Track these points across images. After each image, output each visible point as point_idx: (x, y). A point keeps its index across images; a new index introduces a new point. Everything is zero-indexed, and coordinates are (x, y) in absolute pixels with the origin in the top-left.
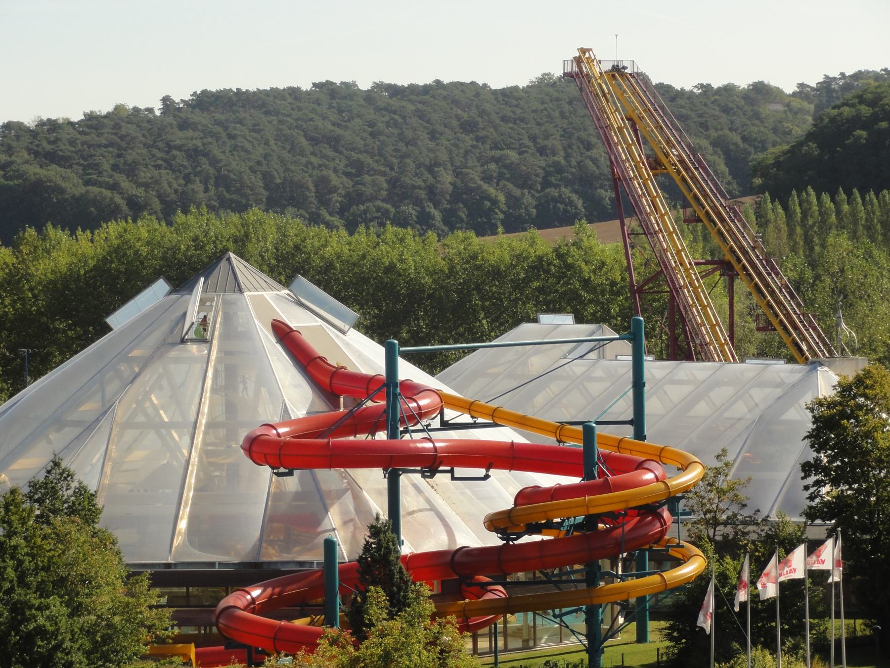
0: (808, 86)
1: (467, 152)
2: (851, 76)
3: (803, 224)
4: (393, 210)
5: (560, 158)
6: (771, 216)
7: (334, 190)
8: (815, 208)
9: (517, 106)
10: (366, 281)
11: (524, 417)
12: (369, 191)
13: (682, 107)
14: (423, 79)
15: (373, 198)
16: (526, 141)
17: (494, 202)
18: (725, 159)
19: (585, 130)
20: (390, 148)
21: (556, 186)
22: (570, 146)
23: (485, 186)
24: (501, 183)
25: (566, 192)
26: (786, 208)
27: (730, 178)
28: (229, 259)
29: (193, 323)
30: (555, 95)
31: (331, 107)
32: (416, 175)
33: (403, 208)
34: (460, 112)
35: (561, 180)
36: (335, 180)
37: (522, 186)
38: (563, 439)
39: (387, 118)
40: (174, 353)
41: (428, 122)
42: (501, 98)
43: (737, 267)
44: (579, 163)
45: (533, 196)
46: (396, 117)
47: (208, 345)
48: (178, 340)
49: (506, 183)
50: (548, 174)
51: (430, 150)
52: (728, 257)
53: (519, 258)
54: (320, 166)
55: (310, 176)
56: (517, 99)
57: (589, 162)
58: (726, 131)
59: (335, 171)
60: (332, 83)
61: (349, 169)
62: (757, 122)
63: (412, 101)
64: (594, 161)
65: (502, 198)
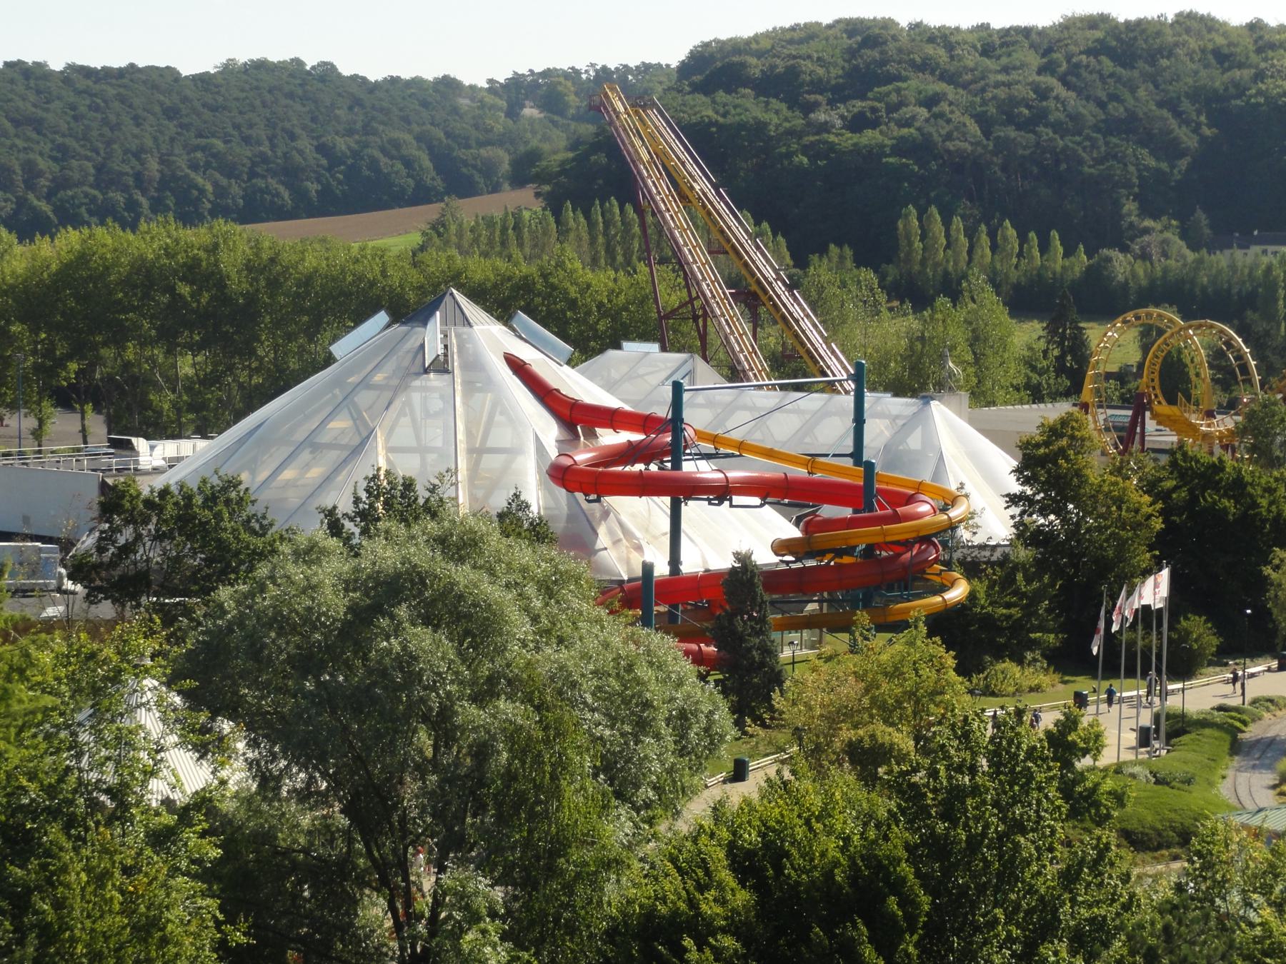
1: (172, 140)
3: (606, 234)
4: (100, 197)
5: (265, 148)
6: (572, 224)
7: (40, 174)
8: (618, 218)
9: (218, 93)
10: (348, 295)
12: (76, 176)
13: (381, 100)
14: (118, 62)
15: (79, 184)
16: (230, 130)
17: (202, 191)
19: (289, 120)
20: (95, 133)
21: (264, 177)
22: (274, 136)
23: (193, 175)
25: (273, 183)
26: (587, 216)
27: (433, 174)
28: (452, 294)
30: (255, 83)
31: (28, 88)
32: (123, 161)
33: (111, 195)
34: (162, 98)
35: (267, 170)
36: (42, 164)
37: (229, 176)
39: (88, 102)
40: (417, 383)
42: (200, 84)
43: (764, 298)
44: (285, 154)
46: (99, 101)
50: (254, 164)
51: (135, 136)
52: (754, 287)
54: (25, 149)
55: (17, 159)
56: (217, 86)
57: (294, 153)
58: (429, 127)
59: (41, 154)
60: (24, 63)
61: (55, 153)
63: (110, 84)
64: (301, 152)
65: (209, 188)
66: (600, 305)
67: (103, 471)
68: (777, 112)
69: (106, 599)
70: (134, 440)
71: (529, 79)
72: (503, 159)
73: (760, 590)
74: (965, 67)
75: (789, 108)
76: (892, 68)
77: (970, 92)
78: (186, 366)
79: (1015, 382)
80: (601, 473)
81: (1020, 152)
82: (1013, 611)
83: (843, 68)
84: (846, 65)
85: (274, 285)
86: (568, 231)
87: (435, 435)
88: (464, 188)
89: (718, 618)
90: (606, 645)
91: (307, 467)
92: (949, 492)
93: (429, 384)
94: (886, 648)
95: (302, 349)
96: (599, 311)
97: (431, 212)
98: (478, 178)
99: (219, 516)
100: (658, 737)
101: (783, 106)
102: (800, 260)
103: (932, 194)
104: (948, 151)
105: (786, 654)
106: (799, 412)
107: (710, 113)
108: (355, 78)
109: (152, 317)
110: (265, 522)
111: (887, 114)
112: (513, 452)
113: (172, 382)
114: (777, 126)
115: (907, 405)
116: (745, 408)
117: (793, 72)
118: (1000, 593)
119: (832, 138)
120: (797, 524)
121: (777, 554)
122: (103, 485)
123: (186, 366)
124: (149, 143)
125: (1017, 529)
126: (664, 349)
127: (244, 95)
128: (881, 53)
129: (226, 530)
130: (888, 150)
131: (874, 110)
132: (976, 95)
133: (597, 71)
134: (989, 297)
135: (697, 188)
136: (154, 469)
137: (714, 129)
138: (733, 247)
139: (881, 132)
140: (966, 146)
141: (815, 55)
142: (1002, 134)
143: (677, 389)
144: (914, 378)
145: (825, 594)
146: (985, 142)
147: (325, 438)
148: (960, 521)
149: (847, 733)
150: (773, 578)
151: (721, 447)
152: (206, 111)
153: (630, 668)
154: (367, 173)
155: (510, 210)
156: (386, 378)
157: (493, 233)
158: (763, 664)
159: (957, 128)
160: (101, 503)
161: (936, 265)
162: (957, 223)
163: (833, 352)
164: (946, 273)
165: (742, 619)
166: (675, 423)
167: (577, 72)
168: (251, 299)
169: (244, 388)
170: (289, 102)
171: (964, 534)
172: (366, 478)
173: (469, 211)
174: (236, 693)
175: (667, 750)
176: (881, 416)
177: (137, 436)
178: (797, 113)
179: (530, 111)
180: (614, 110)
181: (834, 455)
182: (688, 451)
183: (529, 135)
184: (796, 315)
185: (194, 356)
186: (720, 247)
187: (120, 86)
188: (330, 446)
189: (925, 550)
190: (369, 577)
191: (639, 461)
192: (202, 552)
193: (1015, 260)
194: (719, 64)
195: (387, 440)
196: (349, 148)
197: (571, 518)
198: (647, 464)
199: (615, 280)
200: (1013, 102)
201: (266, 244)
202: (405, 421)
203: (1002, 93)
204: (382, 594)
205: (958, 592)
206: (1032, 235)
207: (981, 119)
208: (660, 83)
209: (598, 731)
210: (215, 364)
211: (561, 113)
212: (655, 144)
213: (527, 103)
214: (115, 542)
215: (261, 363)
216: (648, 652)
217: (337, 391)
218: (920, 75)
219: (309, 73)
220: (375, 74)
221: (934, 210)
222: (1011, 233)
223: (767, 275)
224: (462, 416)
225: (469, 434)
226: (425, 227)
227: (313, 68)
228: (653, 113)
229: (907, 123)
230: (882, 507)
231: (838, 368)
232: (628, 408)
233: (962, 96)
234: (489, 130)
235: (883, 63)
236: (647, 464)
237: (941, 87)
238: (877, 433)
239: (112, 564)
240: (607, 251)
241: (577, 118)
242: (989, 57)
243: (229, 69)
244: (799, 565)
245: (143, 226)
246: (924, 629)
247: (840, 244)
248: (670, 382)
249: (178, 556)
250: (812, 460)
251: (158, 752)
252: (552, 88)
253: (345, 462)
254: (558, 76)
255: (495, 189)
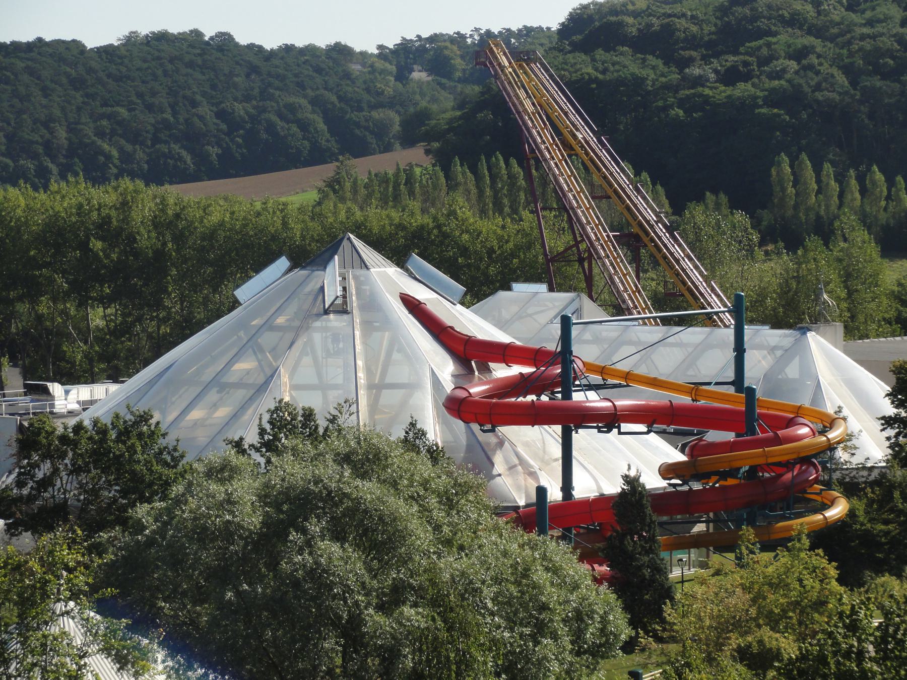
0: (387, 48)
1: (79, 109)
2: (427, 39)
4: (11, 164)
5: (168, 116)
8: (504, 172)
9: (121, 64)
11: (655, 379)
13: (277, 67)
16: (134, 98)
17: (108, 157)
18: (323, 118)
19: (190, 89)
21: (166, 142)
23: (99, 142)
24: (113, 139)
25: (176, 147)
26: (474, 170)
27: (328, 136)
28: (349, 239)
29: (337, 297)
30: (156, 54)
33: (22, 162)
34: (68, 69)
38: (698, 398)
40: (318, 324)
41: (39, 78)
43: (646, 240)
44: (186, 120)
45: (144, 152)
46: (8, 74)
47: (350, 316)
48: (322, 311)
49: (118, 138)
53: (401, 227)
56: (120, 57)
57: (196, 119)
58: (322, 91)
62: (349, 82)
64: (201, 118)
65: (115, 153)
66: (491, 251)
67: (20, 415)
68: (654, 68)
69: (26, 531)
70: (50, 385)
71: (417, 44)
72: (394, 119)
73: (649, 511)
74: (831, 21)
75: (664, 64)
76: (762, 24)
77: (837, 44)
78: (97, 318)
79: (887, 316)
80: (495, 404)
81: (886, 101)
82: (890, 527)
83: (716, 25)
84: (719, 22)
85: (180, 238)
86: (457, 185)
87: (335, 373)
88: (360, 149)
89: (610, 538)
90: (505, 554)
91: (215, 406)
92: (827, 415)
93: (329, 324)
94: (768, 564)
95: (206, 299)
96: (490, 257)
97: (328, 170)
98: (370, 139)
99: (132, 450)
100: (555, 637)
101: (659, 63)
102: (678, 207)
103: (804, 142)
104: (817, 101)
105: (675, 573)
106: (680, 345)
107: (590, 70)
108: (251, 46)
109: (64, 272)
110: (176, 454)
111: (759, 66)
112: (411, 387)
113: (84, 333)
114: (654, 81)
115: (786, 336)
116: (630, 343)
117: (668, 31)
118: (878, 510)
119: (707, 91)
120: (682, 451)
121: (664, 478)
122: (21, 428)
123: (97, 318)
124: (57, 112)
125: (893, 449)
126: (551, 289)
127: (146, 65)
128: (752, 10)
129: (139, 462)
130: (760, 102)
131: (746, 64)
132: (842, 48)
133: (481, 35)
134: (861, 235)
135: (580, 136)
136: (69, 412)
137: (594, 86)
138: (615, 191)
139: (754, 85)
140: (835, 96)
141: (689, 13)
142: (868, 84)
143: (566, 323)
144: (792, 312)
145: (711, 515)
146: (852, 92)
147: (231, 378)
148: (839, 443)
149: (735, 641)
150: (660, 500)
151: (608, 378)
152: (110, 81)
153: (526, 574)
154: (265, 136)
155: (402, 167)
156: (288, 320)
157: (386, 189)
158: (652, 581)
159: (825, 80)
160: (19, 441)
161: (808, 209)
162: (828, 168)
163: (713, 290)
164: (819, 217)
165: (632, 539)
166: (565, 355)
167: (462, 37)
168: (160, 255)
169: (153, 338)
170: (190, 71)
171: (841, 455)
172: (269, 411)
173: (363, 168)
174: (153, 605)
175: (564, 649)
176: (759, 347)
177: (53, 381)
178: (673, 69)
179: (419, 75)
180: (499, 64)
181: (717, 384)
182: (577, 382)
183: (418, 97)
184: (676, 255)
185: (105, 308)
186: (604, 193)
187: (28, 59)
188: (238, 385)
189: (805, 471)
190: (279, 493)
191: (531, 394)
192: (117, 484)
193: (883, 203)
194: (597, 23)
195: (291, 378)
196: (247, 113)
197: (469, 448)
198: (539, 395)
199: (503, 227)
200: (879, 53)
201: (171, 201)
202: (307, 360)
203: (867, 45)
204: (292, 508)
205: (838, 510)
206: (899, 179)
207: (847, 70)
208: (542, 45)
209: (497, 634)
210: (124, 315)
211: (448, 75)
212: (537, 97)
213: (415, 67)
214: (33, 476)
215: (169, 313)
216: (544, 557)
217: (242, 334)
218: (790, 30)
219: (207, 43)
220: (270, 43)
221: (804, 156)
222: (879, 176)
223: (648, 218)
224: (362, 351)
225: (369, 371)
226: (321, 184)
227: (212, 38)
228: (536, 67)
229: (778, 75)
230: (764, 431)
231: (717, 304)
232: (518, 343)
233: (830, 49)
234: (380, 93)
235: (755, 18)
236: (539, 395)
237: (809, 40)
238: (757, 365)
239: (30, 499)
240: (494, 204)
241: (463, 80)
242: (854, 11)
243: (131, 41)
244: (685, 488)
245: (54, 187)
246: (806, 542)
247: (715, 192)
248: (559, 319)
249: (93, 489)
250: (695, 388)
251: (81, 657)
252: (439, 52)
253: (251, 400)
254: (445, 41)
255: (387, 148)
